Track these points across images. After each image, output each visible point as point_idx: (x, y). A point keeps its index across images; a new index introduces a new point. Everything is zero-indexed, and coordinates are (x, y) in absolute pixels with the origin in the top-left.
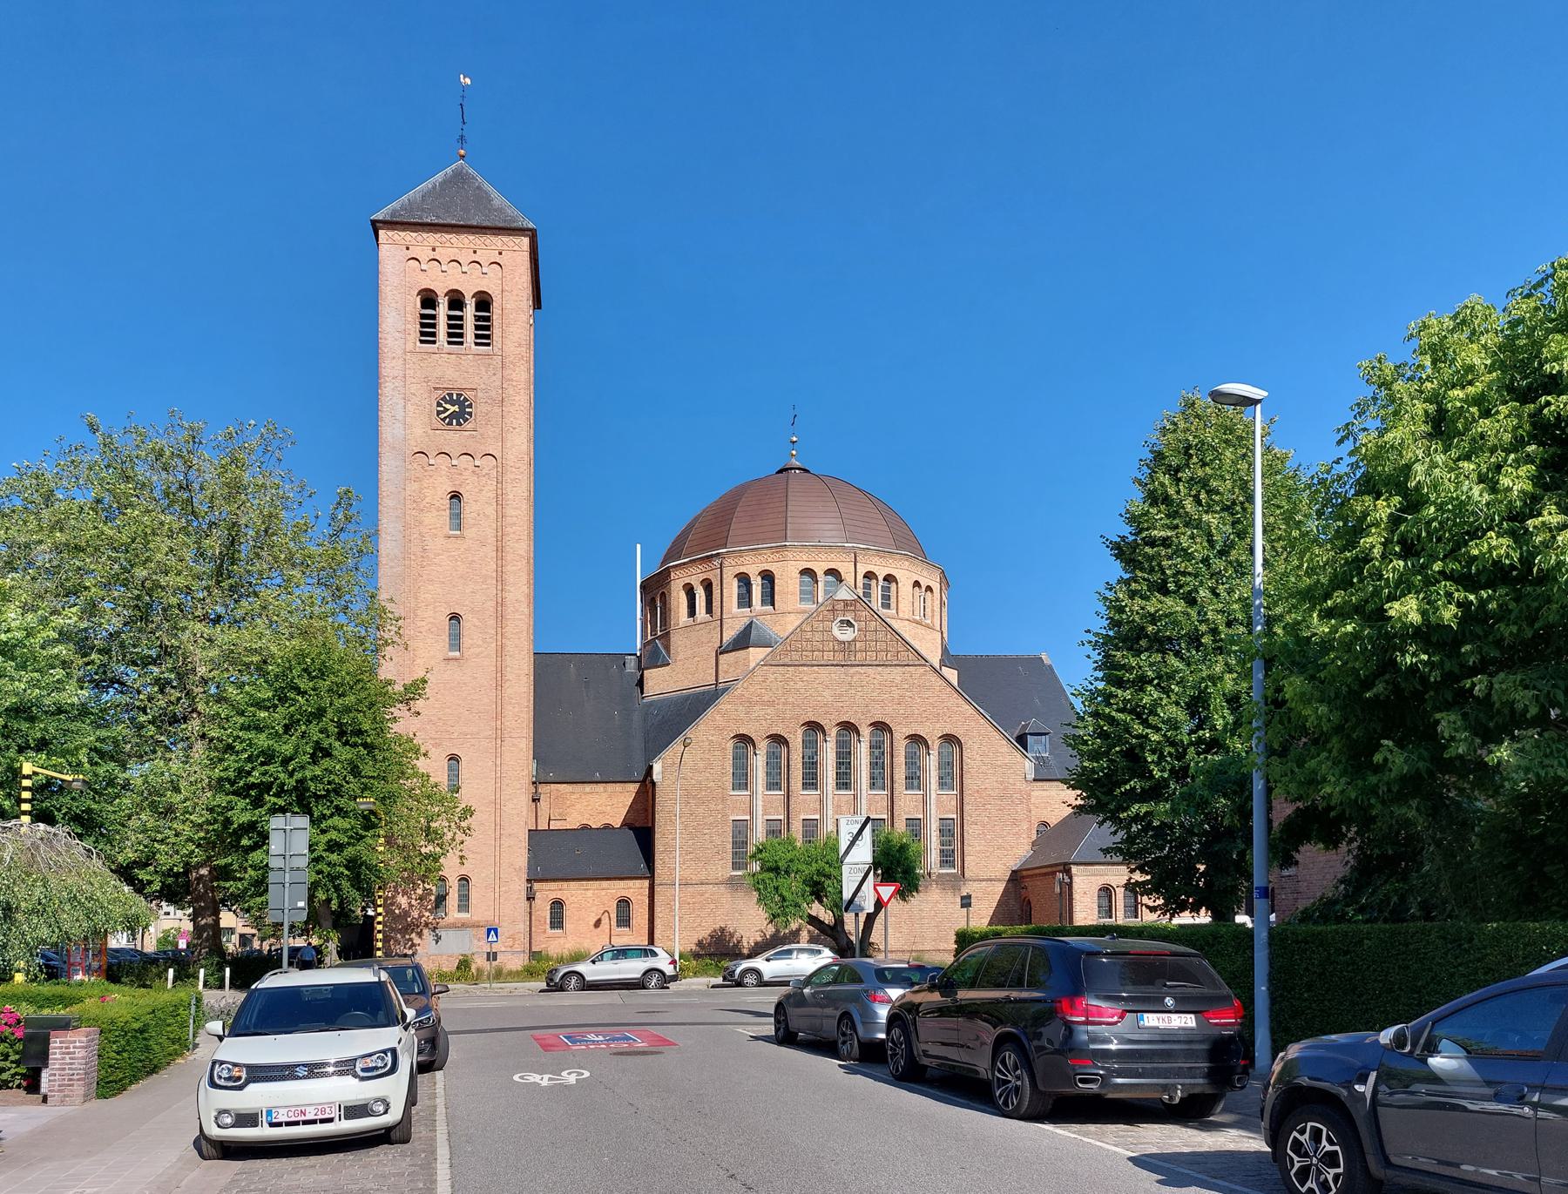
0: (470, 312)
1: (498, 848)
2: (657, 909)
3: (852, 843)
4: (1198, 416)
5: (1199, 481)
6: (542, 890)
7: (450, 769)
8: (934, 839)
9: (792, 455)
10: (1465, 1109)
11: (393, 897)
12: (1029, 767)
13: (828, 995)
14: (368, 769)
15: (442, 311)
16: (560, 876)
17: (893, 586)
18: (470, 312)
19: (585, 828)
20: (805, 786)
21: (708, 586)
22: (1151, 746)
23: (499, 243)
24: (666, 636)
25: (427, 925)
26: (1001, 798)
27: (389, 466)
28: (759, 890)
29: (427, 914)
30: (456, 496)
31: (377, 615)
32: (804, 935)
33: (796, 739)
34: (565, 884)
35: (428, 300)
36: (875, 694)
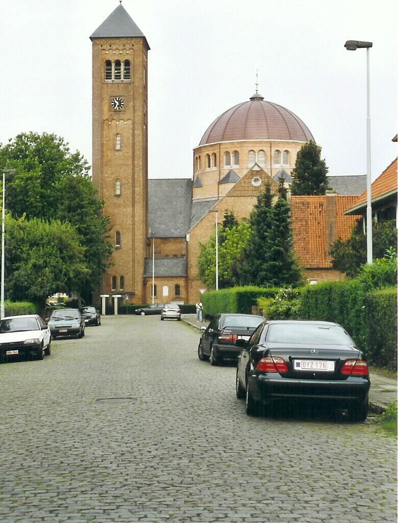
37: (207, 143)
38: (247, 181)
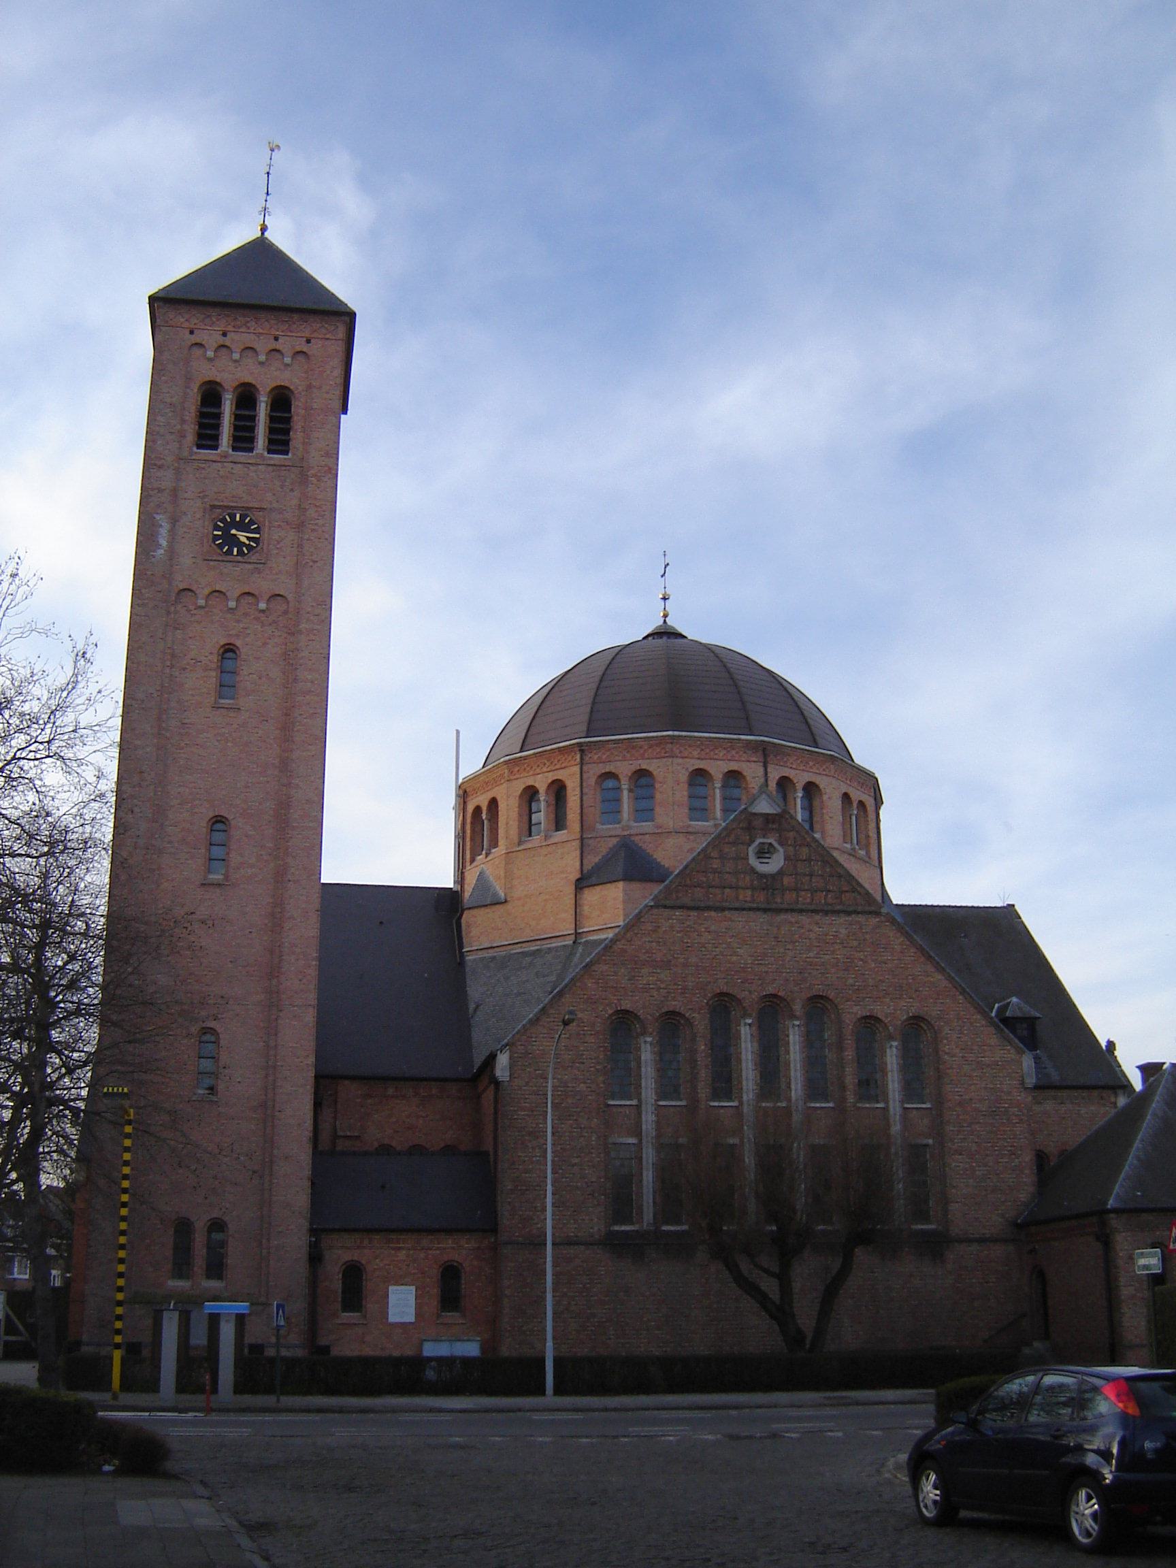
10: (784, 1437)
30: (229, 650)
33: (701, 1023)
36: (811, 954)
37: (521, 752)
38: (731, 851)
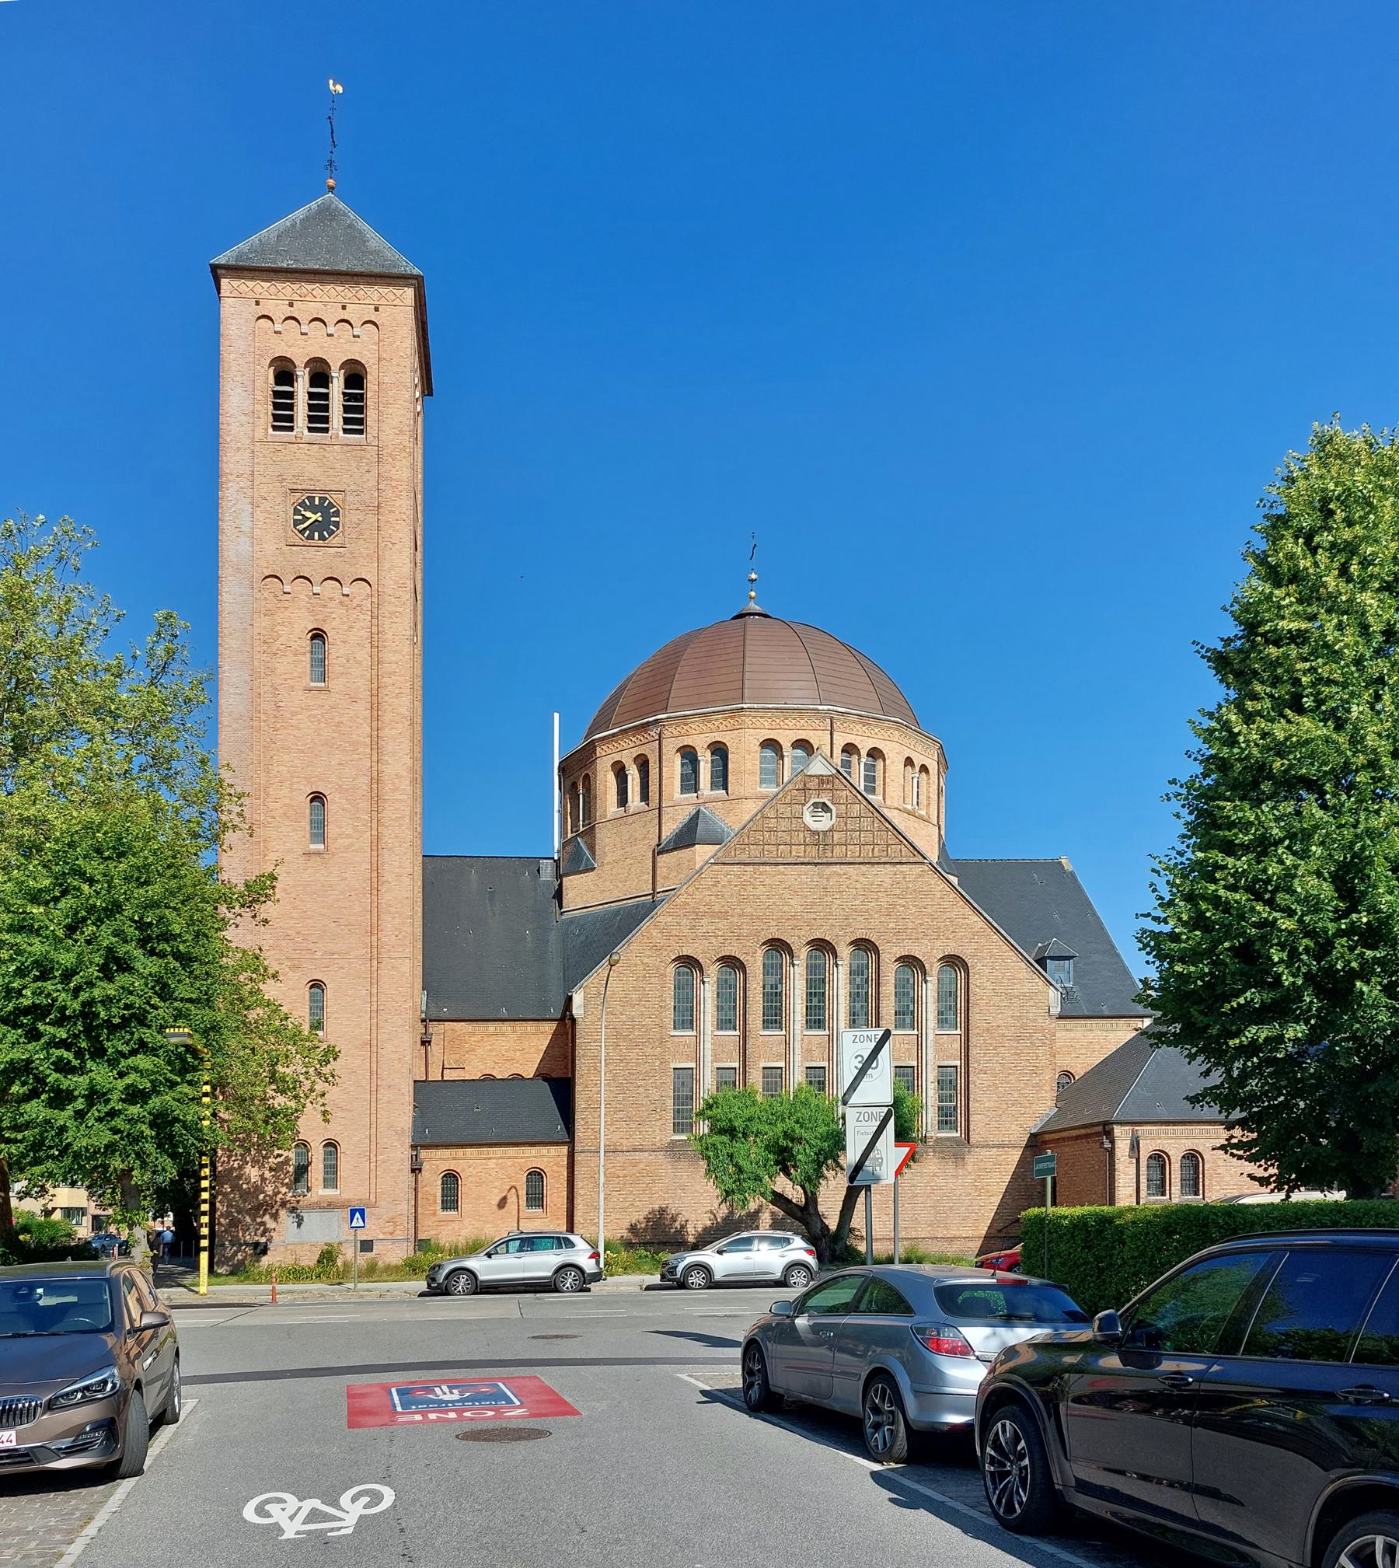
0: (337, 388)
1: (374, 1104)
2: (578, 1184)
3: (862, 1073)
4: (1340, 456)
5: (1344, 549)
6: (431, 1159)
7: (312, 999)
8: (931, 1093)
9: (751, 598)
11: (240, 1167)
12: (1054, 997)
13: (842, 1332)
14: (184, 990)
15: (302, 387)
16: (454, 1140)
17: (880, 764)
18: (337, 388)
19: (489, 1079)
20: (767, 1024)
21: (643, 764)
22: (1279, 938)
23: (376, 296)
24: (590, 831)
25: (283, 1204)
26: (1018, 1038)
27: (232, 593)
28: (708, 1158)
29: (284, 1190)
30: (318, 635)
31: (212, 795)
32: (766, 1218)
33: (755, 962)
34: (460, 1152)
35: (284, 374)
36: (857, 902)
38: (787, 811)
